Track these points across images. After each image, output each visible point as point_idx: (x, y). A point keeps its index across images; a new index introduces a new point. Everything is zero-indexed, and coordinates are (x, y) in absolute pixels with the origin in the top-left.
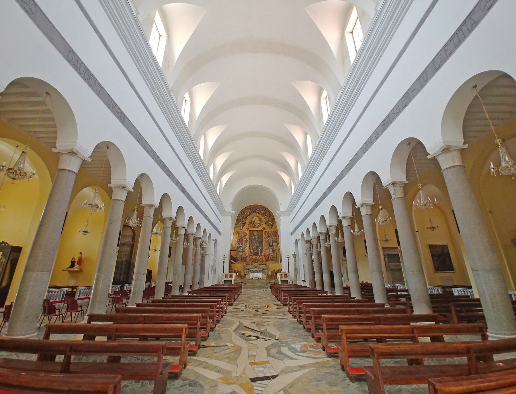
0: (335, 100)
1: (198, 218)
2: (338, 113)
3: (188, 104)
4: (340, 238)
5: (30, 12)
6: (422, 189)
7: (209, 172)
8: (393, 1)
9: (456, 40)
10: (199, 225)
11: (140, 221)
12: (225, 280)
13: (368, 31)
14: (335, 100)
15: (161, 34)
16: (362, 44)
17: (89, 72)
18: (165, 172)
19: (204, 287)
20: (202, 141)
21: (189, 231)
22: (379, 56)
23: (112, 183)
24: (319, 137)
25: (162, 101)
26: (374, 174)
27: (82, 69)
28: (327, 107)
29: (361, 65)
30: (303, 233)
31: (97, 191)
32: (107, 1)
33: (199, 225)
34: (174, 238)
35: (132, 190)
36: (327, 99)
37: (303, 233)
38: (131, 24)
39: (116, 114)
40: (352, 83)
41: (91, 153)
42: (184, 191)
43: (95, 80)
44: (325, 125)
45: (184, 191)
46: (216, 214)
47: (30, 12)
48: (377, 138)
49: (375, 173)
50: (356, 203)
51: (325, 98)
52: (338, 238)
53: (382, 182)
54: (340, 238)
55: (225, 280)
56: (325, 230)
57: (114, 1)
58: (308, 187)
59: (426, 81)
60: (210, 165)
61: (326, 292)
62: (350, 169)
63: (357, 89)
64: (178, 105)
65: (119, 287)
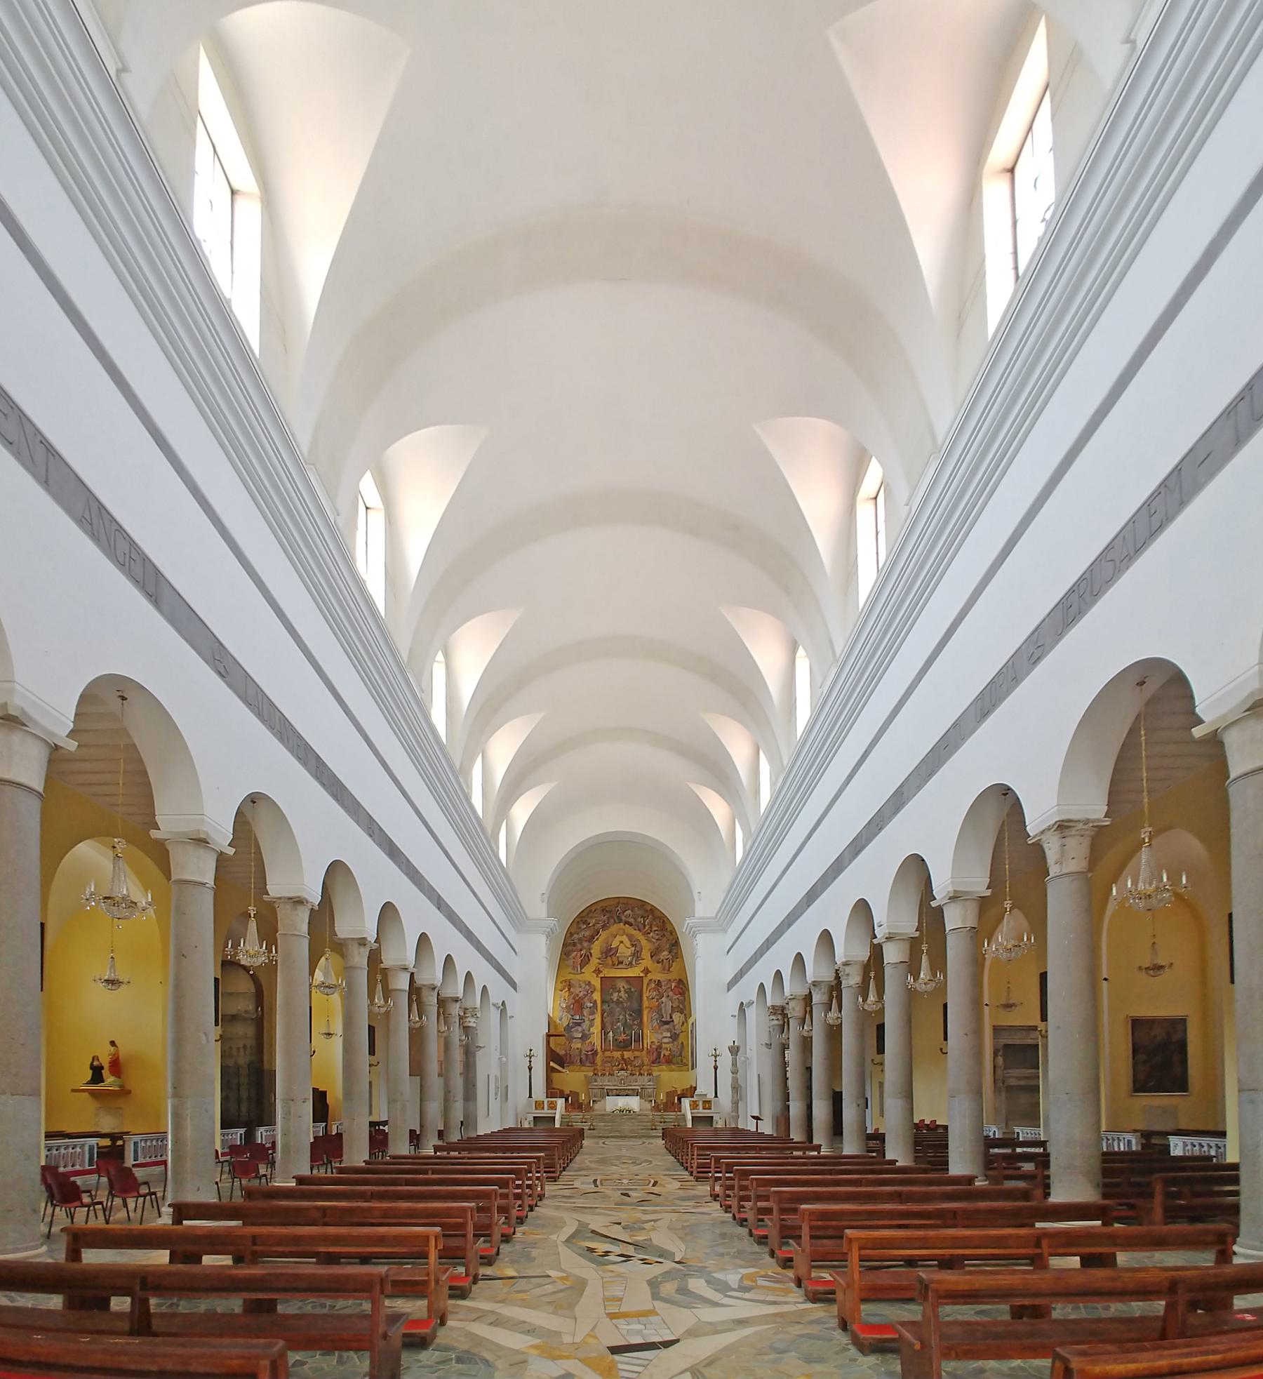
4: (872, 997)
7: (470, 787)
10: (423, 939)
24: (838, 655)
34: (379, 1000)
41: (72, 720)
42: (393, 852)
44: (863, 610)
46: (499, 928)
50: (934, 892)
51: (874, 496)
53: (1025, 822)
54: (872, 997)
56: (863, 954)
62: (889, 818)
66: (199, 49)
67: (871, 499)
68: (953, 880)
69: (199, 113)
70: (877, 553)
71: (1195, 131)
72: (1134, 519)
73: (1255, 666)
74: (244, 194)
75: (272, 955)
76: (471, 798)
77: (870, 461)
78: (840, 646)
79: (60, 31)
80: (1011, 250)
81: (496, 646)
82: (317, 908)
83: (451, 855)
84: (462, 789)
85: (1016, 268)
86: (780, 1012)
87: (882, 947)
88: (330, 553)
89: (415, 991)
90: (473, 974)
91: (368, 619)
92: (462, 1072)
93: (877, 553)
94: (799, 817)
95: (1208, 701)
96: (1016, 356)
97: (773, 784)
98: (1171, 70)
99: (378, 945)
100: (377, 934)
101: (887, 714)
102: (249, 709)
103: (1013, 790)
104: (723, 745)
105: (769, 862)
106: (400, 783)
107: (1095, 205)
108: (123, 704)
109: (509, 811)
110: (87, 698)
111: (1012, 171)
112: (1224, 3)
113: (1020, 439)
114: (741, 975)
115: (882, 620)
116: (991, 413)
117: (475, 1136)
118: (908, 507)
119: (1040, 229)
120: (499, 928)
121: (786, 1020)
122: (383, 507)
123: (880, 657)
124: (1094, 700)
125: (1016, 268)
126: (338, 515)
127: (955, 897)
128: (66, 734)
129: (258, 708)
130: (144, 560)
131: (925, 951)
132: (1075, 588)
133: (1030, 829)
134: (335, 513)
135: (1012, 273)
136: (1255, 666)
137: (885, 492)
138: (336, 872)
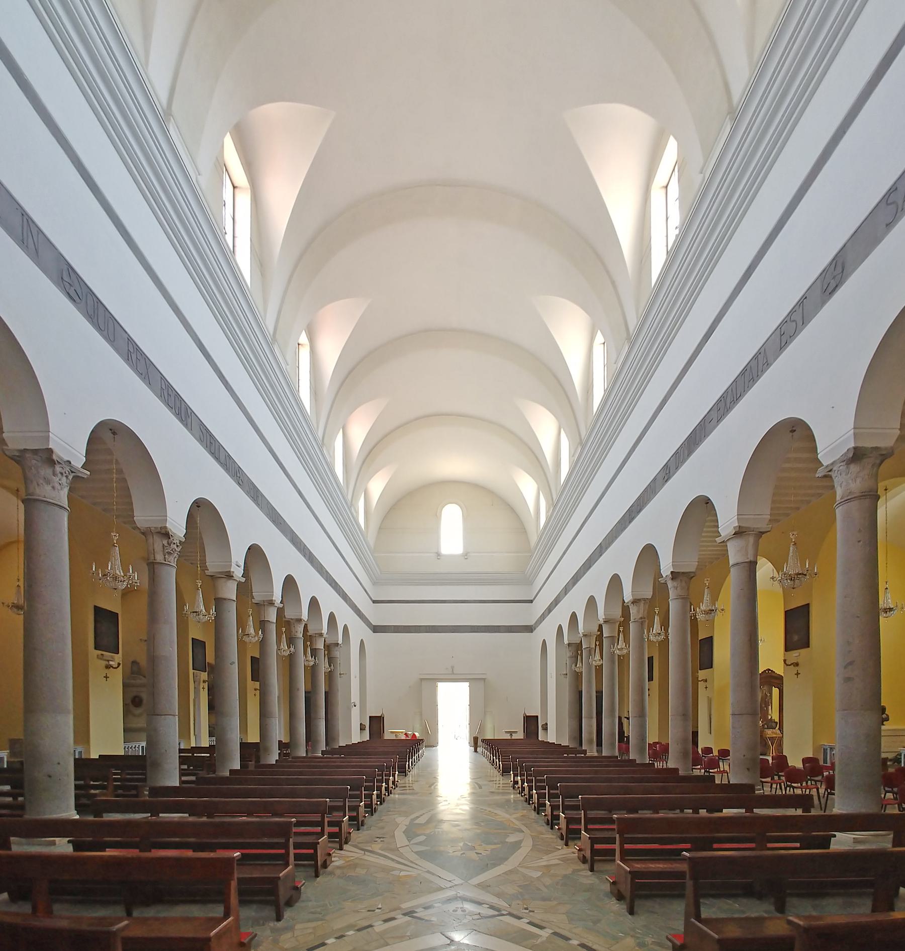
0: (615, 363)
1: (330, 603)
2: (709, 217)
3: (244, 200)
4: (657, 628)
5: (76, 298)
6: (708, 588)
7: (357, 512)
8: (814, 3)
9: (797, 317)
10: (332, 617)
11: (315, 659)
12: (537, 717)
13: (747, 86)
14: (615, 363)
15: (235, 185)
16: (680, 232)
17: (80, 280)
18: (300, 552)
19: (340, 745)
20: (304, 354)
21: (289, 614)
22: (686, 310)
23: (255, 597)
24: (583, 438)
25: (280, 408)
26: (708, 503)
27: (222, 458)
28: (667, 219)
29: (652, 325)
30: (544, 640)
31: (115, 545)
32: (48, 2)
33: (332, 617)
34: (284, 646)
35: (243, 580)
36: (605, 344)
37: (544, 640)
38: (228, 281)
39: (178, 414)
40: (646, 339)
41: (85, 455)
42: (255, 495)
43: (145, 359)
44: (595, 415)
45: (255, 495)
46: (361, 584)
47: (76, 298)
48: (666, 481)
49: (710, 499)
50: (661, 571)
51: (665, 184)
52: (576, 666)
53: (817, 450)
54: (657, 628)
55: (537, 717)
56: (617, 613)
57: (69, 2)
58: (556, 546)
59: (728, 410)
60: (333, 438)
61: (585, 752)
62: (638, 513)
63: (714, 244)
64: (288, 370)
65: (143, 747)
66: (339, 430)
67: (663, 187)
68: (857, 431)
69: (225, 165)
70: (667, 236)
71: (848, 15)
72: (786, 319)
73: (850, 430)
74: (240, 188)
75: (128, 574)
76: (334, 467)
77: (669, 139)
78: (633, 323)
79: (257, 342)
80: (665, 235)
81: (351, 330)
82: (183, 540)
83: (321, 519)
84: (352, 514)
85: (667, 246)
86: (576, 648)
87: (602, 626)
88: (226, 279)
89: (309, 638)
90: (348, 626)
91: (255, 329)
92: (795, 809)
93: (667, 236)
94: (608, 455)
95: (825, 451)
96: (712, 203)
97: (547, 512)
98: (788, 56)
99: (282, 605)
100: (282, 597)
101: (658, 404)
102: (221, 466)
103: (711, 501)
104: (600, 193)
105: (555, 544)
106: (306, 501)
107: (733, 161)
108: (114, 438)
109: (368, 482)
110: (95, 439)
111: (666, 187)
112: (827, 2)
113: (788, 131)
114: (566, 592)
115: (613, 407)
116: (678, 277)
117: (338, 747)
118: (702, 175)
119: (674, 238)
120: (361, 584)
121: (579, 652)
122: (249, 186)
123: (629, 401)
124: (609, 584)
125: (667, 246)
126: (199, 174)
127: (635, 602)
128: (81, 466)
129: (226, 465)
130: (23, 215)
131: (657, 613)
132: (679, 451)
133: (820, 457)
134: (197, 174)
135: (665, 248)
136: (850, 430)
137: (678, 171)
138: (255, 554)
